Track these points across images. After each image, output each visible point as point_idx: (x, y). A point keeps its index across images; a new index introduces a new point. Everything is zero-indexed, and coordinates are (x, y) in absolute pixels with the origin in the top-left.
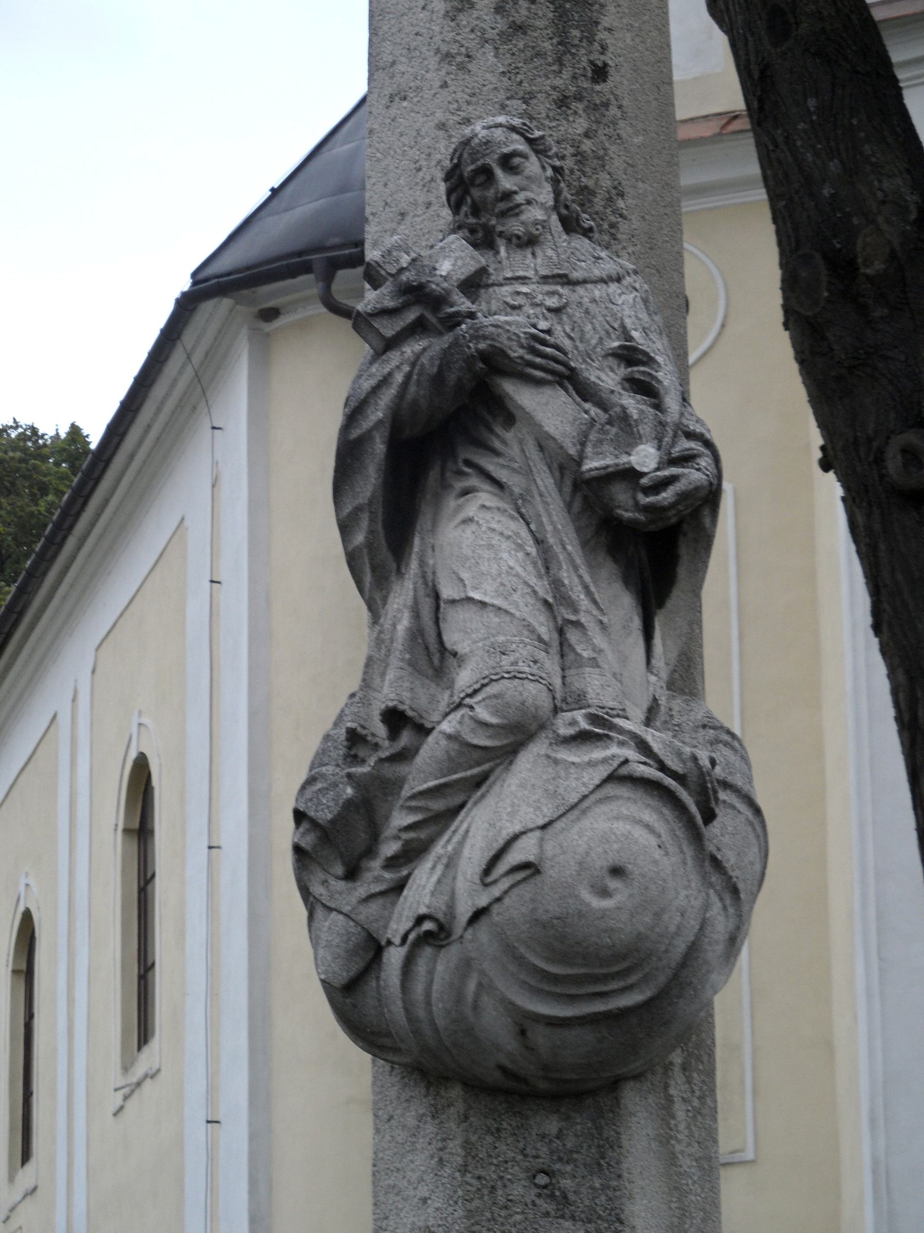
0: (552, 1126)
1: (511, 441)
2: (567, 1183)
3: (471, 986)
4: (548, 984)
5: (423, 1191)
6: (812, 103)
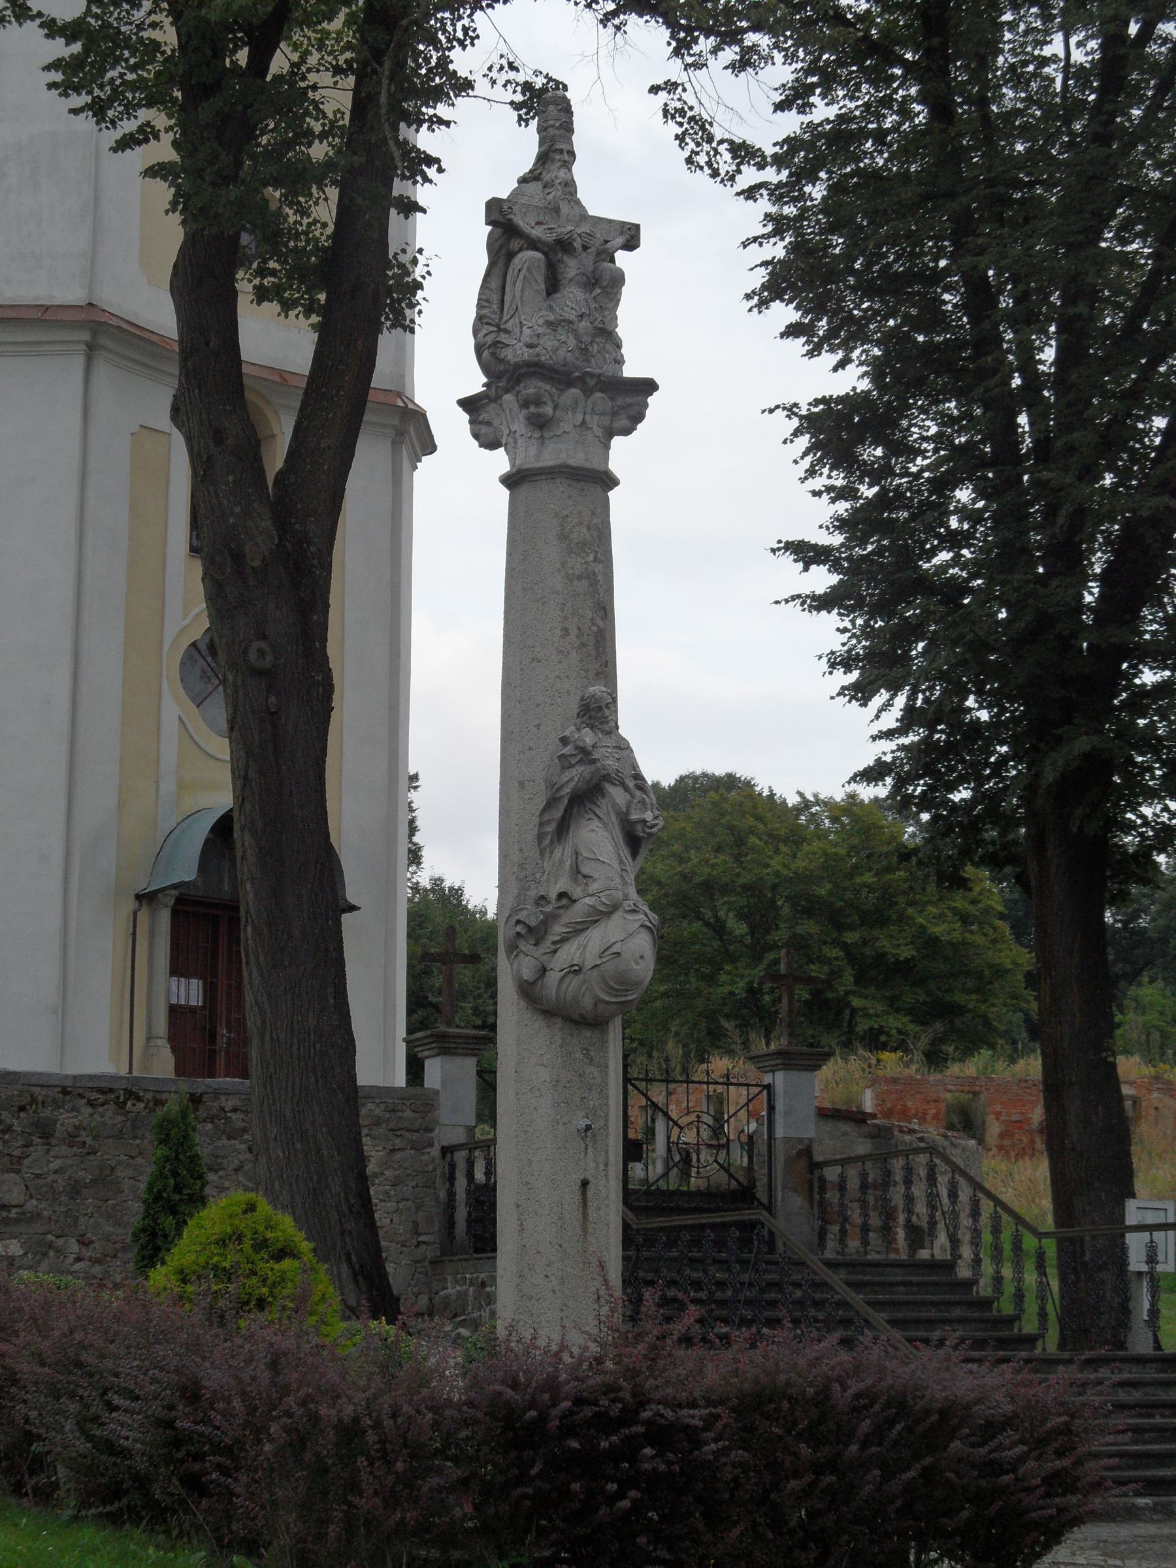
0: (588, 1034)
1: (604, 803)
2: (592, 1053)
3: (584, 989)
4: (612, 990)
5: (541, 1052)
6: (231, 478)
